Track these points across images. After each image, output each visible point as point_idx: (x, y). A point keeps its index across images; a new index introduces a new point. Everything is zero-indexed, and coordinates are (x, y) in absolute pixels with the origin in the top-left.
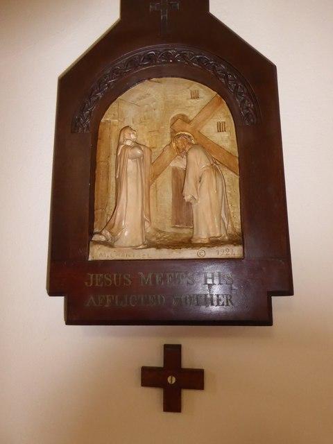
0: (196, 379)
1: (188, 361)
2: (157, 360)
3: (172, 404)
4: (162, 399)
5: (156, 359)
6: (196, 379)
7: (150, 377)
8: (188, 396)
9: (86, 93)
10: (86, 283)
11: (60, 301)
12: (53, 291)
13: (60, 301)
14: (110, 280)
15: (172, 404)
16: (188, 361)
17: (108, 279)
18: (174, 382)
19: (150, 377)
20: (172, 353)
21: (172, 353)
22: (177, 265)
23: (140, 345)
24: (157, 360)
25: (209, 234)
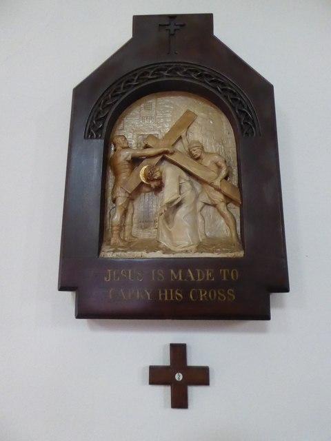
0: (201, 376)
1: (193, 360)
2: (163, 360)
3: (180, 401)
4: (231, 321)
5: (162, 359)
6: (201, 376)
7: (157, 376)
8: (194, 392)
9: (103, 102)
10: (106, 279)
14: (177, 293)
15: (180, 401)
16: (193, 360)
17: (230, 294)
18: (181, 379)
19: (157, 376)
20: (178, 351)
21: (178, 351)
22: (73, 167)
24: (163, 360)
25: (157, 103)
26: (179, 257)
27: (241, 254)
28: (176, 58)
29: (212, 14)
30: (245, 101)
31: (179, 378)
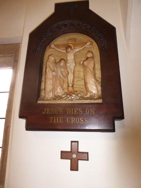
0: (85, 156)
3: (74, 167)
6: (85, 156)
7: (64, 155)
10: (43, 112)
11: (23, 122)
12: (21, 117)
13: (23, 122)
15: (74, 167)
23: (62, 140)
26: (56, 103)
27: (100, 101)
28: (77, 20)
29: (19, 118)
30: (105, 36)
31: (74, 157)
